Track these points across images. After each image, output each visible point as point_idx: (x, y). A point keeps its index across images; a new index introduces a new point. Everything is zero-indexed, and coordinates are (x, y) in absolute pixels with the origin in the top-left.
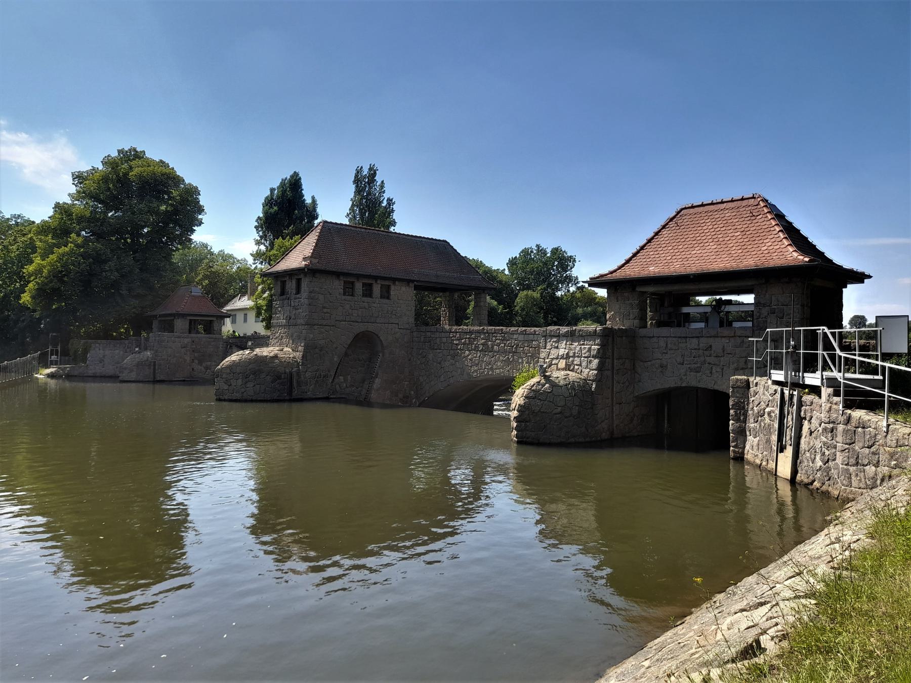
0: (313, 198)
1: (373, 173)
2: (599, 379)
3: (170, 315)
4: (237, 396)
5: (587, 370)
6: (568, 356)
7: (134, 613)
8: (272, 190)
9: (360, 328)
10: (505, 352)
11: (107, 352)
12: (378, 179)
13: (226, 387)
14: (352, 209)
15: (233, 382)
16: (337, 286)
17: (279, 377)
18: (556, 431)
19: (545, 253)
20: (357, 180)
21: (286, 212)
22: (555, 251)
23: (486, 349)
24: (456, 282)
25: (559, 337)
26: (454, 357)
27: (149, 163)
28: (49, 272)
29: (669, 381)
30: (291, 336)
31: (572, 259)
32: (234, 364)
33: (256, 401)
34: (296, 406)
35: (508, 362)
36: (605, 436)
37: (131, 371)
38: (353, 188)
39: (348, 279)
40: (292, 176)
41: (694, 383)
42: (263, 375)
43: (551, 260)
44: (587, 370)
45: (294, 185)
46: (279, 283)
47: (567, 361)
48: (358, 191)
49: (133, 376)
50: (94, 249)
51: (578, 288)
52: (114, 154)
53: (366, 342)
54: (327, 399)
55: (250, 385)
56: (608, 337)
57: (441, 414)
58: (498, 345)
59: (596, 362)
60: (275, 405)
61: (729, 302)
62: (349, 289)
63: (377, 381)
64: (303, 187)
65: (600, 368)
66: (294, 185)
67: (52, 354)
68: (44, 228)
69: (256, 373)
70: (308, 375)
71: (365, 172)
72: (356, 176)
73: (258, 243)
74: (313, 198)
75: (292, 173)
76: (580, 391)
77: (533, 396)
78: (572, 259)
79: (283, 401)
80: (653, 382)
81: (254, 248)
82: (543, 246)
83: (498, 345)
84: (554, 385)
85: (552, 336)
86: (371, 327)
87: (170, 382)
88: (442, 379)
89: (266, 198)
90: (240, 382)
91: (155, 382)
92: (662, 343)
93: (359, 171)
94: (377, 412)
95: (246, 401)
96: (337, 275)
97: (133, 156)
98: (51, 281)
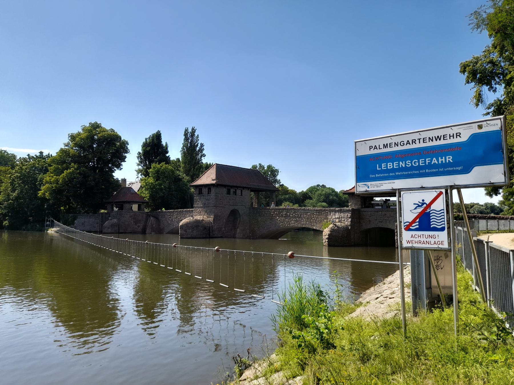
0: (166, 143)
1: (194, 131)
2: (351, 225)
3: (121, 202)
4: (189, 236)
5: (347, 222)
6: (339, 218)
7: (107, 345)
8: (146, 139)
9: (232, 208)
10: (295, 217)
11: (86, 220)
12: (196, 134)
13: (185, 233)
14: (183, 148)
15: (188, 231)
16: (225, 190)
17: (205, 228)
18: (339, 242)
19: (264, 168)
20: (186, 135)
21: (154, 149)
22: (269, 167)
23: (286, 216)
24: (261, 188)
25: (335, 211)
26: (271, 219)
27: (105, 131)
28: (62, 181)
29: (372, 226)
30: (206, 212)
31: (277, 171)
32: (187, 225)
33: (197, 238)
34: (211, 240)
35: (297, 221)
36: (353, 244)
37: (109, 228)
38: (184, 137)
39: (228, 188)
40: (157, 133)
41: (380, 226)
42: (200, 228)
43: (267, 170)
44: (347, 222)
45: (158, 137)
46: (198, 189)
47: (340, 219)
48: (186, 139)
49: (110, 230)
50: (83, 171)
51: (280, 185)
52: (88, 125)
53: (234, 213)
54: (222, 237)
55: (195, 232)
56: (353, 211)
57: (265, 241)
58: (292, 214)
59: (350, 220)
60: (204, 240)
61: (389, 200)
62: (229, 193)
63: (238, 230)
64: (162, 138)
65: (351, 222)
66: (158, 137)
67: (47, 221)
68: (54, 160)
69: (197, 226)
70: (215, 227)
71: (190, 130)
72: (185, 132)
73: (138, 165)
74: (166, 143)
75: (157, 131)
76: (346, 229)
77: (332, 231)
78: (277, 171)
79: (207, 238)
80: (366, 226)
81: (137, 168)
82: (263, 164)
83: (292, 214)
84: (338, 227)
85: (332, 211)
86: (236, 208)
87: (125, 233)
88: (266, 228)
89: (144, 143)
90: (190, 230)
91: (119, 233)
92: (369, 213)
93: (186, 130)
94: (238, 240)
95: (193, 238)
96: (225, 186)
97: (96, 126)
98: (64, 186)
